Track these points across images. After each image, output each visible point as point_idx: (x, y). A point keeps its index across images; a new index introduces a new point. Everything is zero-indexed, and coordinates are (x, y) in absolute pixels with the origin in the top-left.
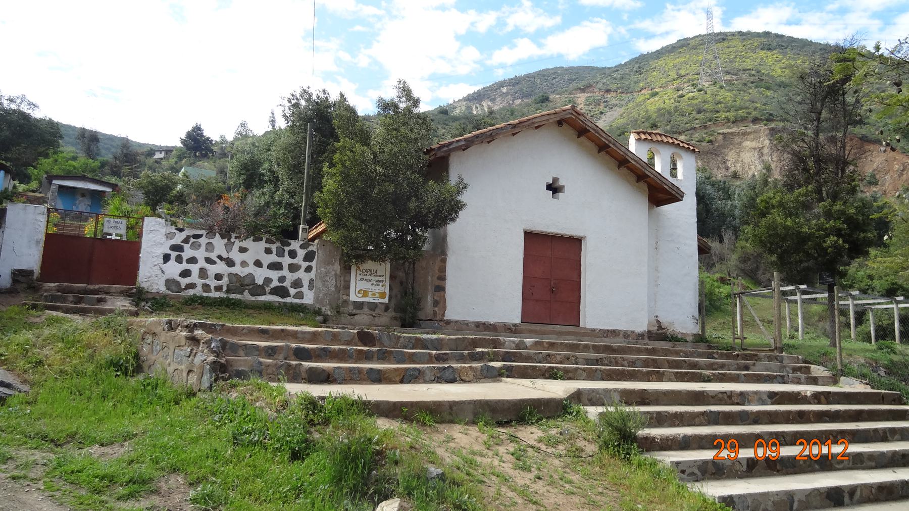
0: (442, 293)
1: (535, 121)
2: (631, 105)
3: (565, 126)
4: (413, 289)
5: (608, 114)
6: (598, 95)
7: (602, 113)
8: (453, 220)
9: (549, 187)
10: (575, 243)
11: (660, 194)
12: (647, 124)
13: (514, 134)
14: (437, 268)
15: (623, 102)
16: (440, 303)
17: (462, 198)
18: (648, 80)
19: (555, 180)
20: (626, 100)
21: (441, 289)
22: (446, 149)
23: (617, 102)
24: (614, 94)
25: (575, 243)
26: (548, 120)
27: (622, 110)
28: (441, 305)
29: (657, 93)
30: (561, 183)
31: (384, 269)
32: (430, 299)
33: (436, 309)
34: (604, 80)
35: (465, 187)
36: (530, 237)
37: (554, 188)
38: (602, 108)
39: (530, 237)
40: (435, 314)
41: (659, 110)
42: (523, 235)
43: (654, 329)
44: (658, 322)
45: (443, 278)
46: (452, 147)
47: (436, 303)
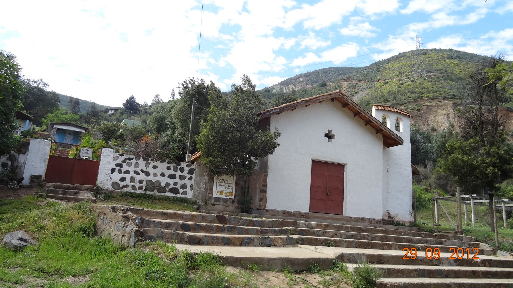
0: (265, 194)
2: (373, 89)
3: (336, 101)
5: (360, 93)
6: (354, 83)
7: (356, 93)
8: (272, 153)
9: (326, 135)
10: (340, 167)
11: (390, 140)
12: (382, 99)
13: (307, 106)
15: (369, 87)
16: (263, 199)
17: (277, 141)
18: (383, 75)
19: (330, 131)
20: (370, 86)
21: (264, 191)
22: (268, 113)
23: (365, 87)
24: (363, 83)
25: (340, 167)
26: (326, 98)
27: (368, 91)
28: (264, 201)
29: (388, 82)
30: (333, 133)
31: (232, 179)
32: (257, 198)
33: (261, 203)
34: (358, 75)
35: (279, 135)
36: (315, 163)
37: (329, 136)
38: (356, 90)
39: (315, 163)
40: (260, 205)
41: (389, 92)
43: (386, 218)
44: (389, 214)
45: (265, 185)
46: (272, 112)
47: (261, 200)
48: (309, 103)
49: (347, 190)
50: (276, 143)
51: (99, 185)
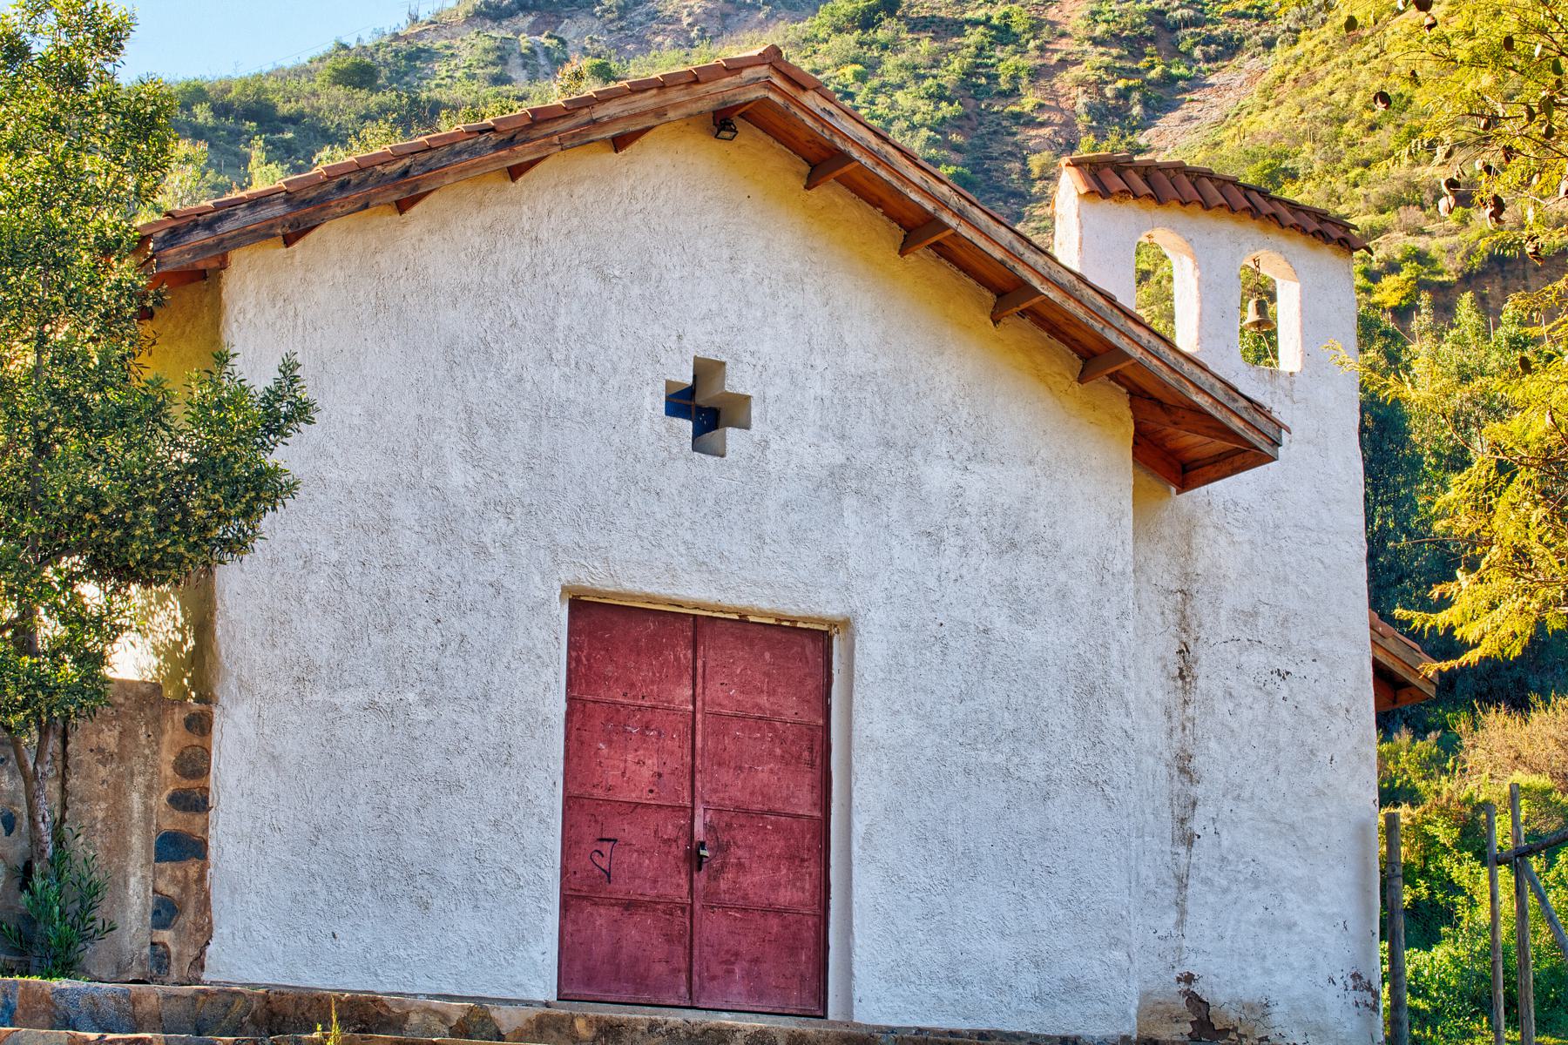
1: (600, 112)
3: (747, 135)
4: (59, 842)
8: (237, 546)
9: (681, 402)
10: (806, 651)
11: (1184, 438)
13: (515, 173)
14: (168, 757)
17: (284, 456)
19: (707, 370)
21: (182, 847)
22: (200, 237)
25: (806, 651)
26: (660, 112)
28: (189, 917)
30: (736, 382)
31: (1403, 730)
33: (166, 936)
35: (303, 412)
42: (563, 613)
44: (1195, 1001)
46: (227, 227)
47: (165, 912)
48: (523, 153)
49: (859, 828)
50: (275, 472)
51: (513, 1028)
